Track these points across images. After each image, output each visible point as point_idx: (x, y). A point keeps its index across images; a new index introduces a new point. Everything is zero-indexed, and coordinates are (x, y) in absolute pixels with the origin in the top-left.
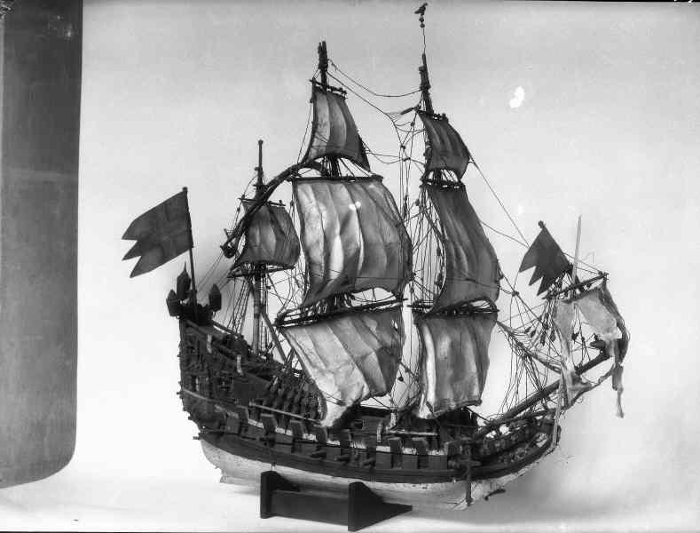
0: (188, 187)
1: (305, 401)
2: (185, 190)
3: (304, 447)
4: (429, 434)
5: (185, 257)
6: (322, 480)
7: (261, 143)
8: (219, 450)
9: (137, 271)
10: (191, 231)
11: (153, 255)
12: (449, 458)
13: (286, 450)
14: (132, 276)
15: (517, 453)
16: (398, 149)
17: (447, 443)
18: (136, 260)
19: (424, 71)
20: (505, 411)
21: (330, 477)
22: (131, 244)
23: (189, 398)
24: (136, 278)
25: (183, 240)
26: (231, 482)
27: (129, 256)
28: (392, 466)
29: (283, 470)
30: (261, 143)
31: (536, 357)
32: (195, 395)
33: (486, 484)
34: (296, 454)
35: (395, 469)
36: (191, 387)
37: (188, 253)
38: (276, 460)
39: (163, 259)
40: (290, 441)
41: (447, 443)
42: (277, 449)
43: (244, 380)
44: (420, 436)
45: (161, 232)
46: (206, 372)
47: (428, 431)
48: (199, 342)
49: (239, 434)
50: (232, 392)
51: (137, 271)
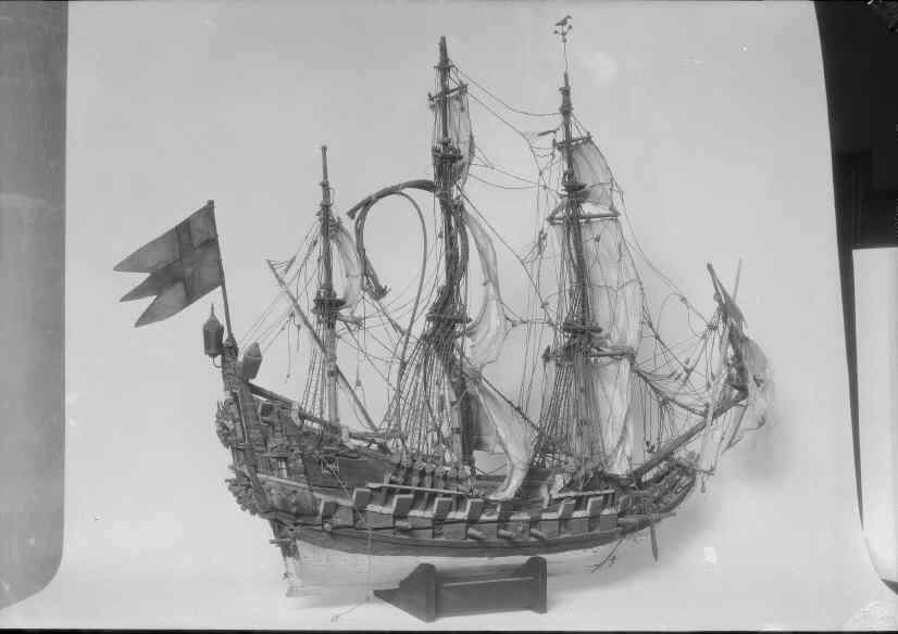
2: (211, 203)
4: (606, 492)
5: (215, 295)
6: (505, 563)
7: (324, 149)
9: (148, 317)
11: (178, 291)
12: (621, 515)
13: (426, 536)
14: (138, 324)
16: (537, 176)
18: (148, 301)
19: (566, 92)
21: (486, 559)
22: (140, 278)
23: (283, 489)
24: (140, 328)
25: (207, 274)
27: (137, 293)
29: (440, 562)
30: (324, 149)
31: (673, 400)
32: (283, 481)
37: (220, 288)
38: (418, 548)
39: (190, 298)
43: (355, 455)
44: (597, 495)
45: (183, 263)
50: (302, 476)
51: (148, 317)
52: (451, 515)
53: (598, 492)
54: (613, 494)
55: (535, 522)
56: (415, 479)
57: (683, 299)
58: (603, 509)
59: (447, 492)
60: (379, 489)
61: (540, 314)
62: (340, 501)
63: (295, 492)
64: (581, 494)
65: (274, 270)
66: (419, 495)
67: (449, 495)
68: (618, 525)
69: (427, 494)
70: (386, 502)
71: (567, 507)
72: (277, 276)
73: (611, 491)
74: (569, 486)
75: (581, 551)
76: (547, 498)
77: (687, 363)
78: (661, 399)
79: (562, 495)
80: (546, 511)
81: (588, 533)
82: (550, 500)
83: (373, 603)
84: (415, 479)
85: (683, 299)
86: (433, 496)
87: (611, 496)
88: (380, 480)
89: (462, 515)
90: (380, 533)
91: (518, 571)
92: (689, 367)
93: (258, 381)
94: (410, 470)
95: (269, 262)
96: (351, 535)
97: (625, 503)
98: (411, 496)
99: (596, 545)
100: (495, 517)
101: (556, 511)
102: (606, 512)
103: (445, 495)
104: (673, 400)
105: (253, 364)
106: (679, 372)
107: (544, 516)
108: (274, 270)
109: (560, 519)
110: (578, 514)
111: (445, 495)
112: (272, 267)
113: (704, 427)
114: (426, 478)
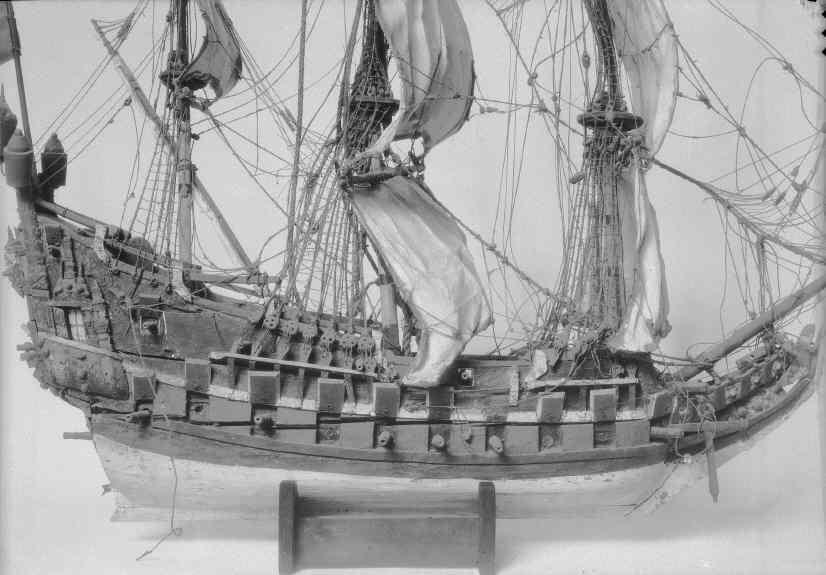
0: (91, 17)
1: (329, 335)
3: (344, 429)
6: (386, 488)
8: (143, 452)
10: (14, 21)
12: (654, 422)
15: (750, 406)
17: (656, 396)
20: (795, 291)
21: (407, 481)
26: (139, 518)
28: (540, 450)
31: (776, 240)
33: (22, 218)
34: (323, 445)
35: (545, 452)
36: (64, 331)
37: (12, 63)
40: (313, 422)
41: (656, 396)
42: (286, 438)
44: (605, 387)
46: (97, 298)
47: (622, 376)
48: (72, 240)
49: (186, 418)
52: (347, 408)
53: (609, 382)
54: (638, 387)
55: (496, 426)
56: (283, 348)
57: (789, 67)
58: (619, 408)
59: (334, 369)
60: (224, 362)
61: (524, 95)
62: (162, 377)
63: (83, 359)
64: (571, 383)
65: (102, 34)
66: (287, 371)
67: (339, 376)
68: (652, 439)
69: (302, 372)
70: (235, 382)
71: (548, 404)
72: (107, 43)
73: (631, 380)
74: (555, 368)
75: (580, 479)
76: (515, 388)
77: (795, 173)
78: (754, 238)
79: (541, 384)
80: (516, 408)
81: (592, 450)
82: (521, 392)
83: (669, 436)
84: (283, 348)
85: (789, 67)
86: (312, 375)
87: (632, 390)
88: (225, 347)
89: (366, 408)
90: (225, 429)
91: (450, 505)
92: (799, 181)
93: (62, 196)
94: (277, 332)
95: (94, 22)
96: (195, 429)
97: (663, 402)
98: (274, 374)
99: (611, 469)
100: (424, 415)
101: (532, 409)
102: (626, 414)
103: (332, 375)
104: (776, 240)
105: (55, 167)
106: (781, 190)
107: (512, 417)
108: (102, 34)
109: (541, 425)
110: (571, 416)
111: (332, 375)
112: (99, 29)
113: (382, 47)
114: (303, 345)
